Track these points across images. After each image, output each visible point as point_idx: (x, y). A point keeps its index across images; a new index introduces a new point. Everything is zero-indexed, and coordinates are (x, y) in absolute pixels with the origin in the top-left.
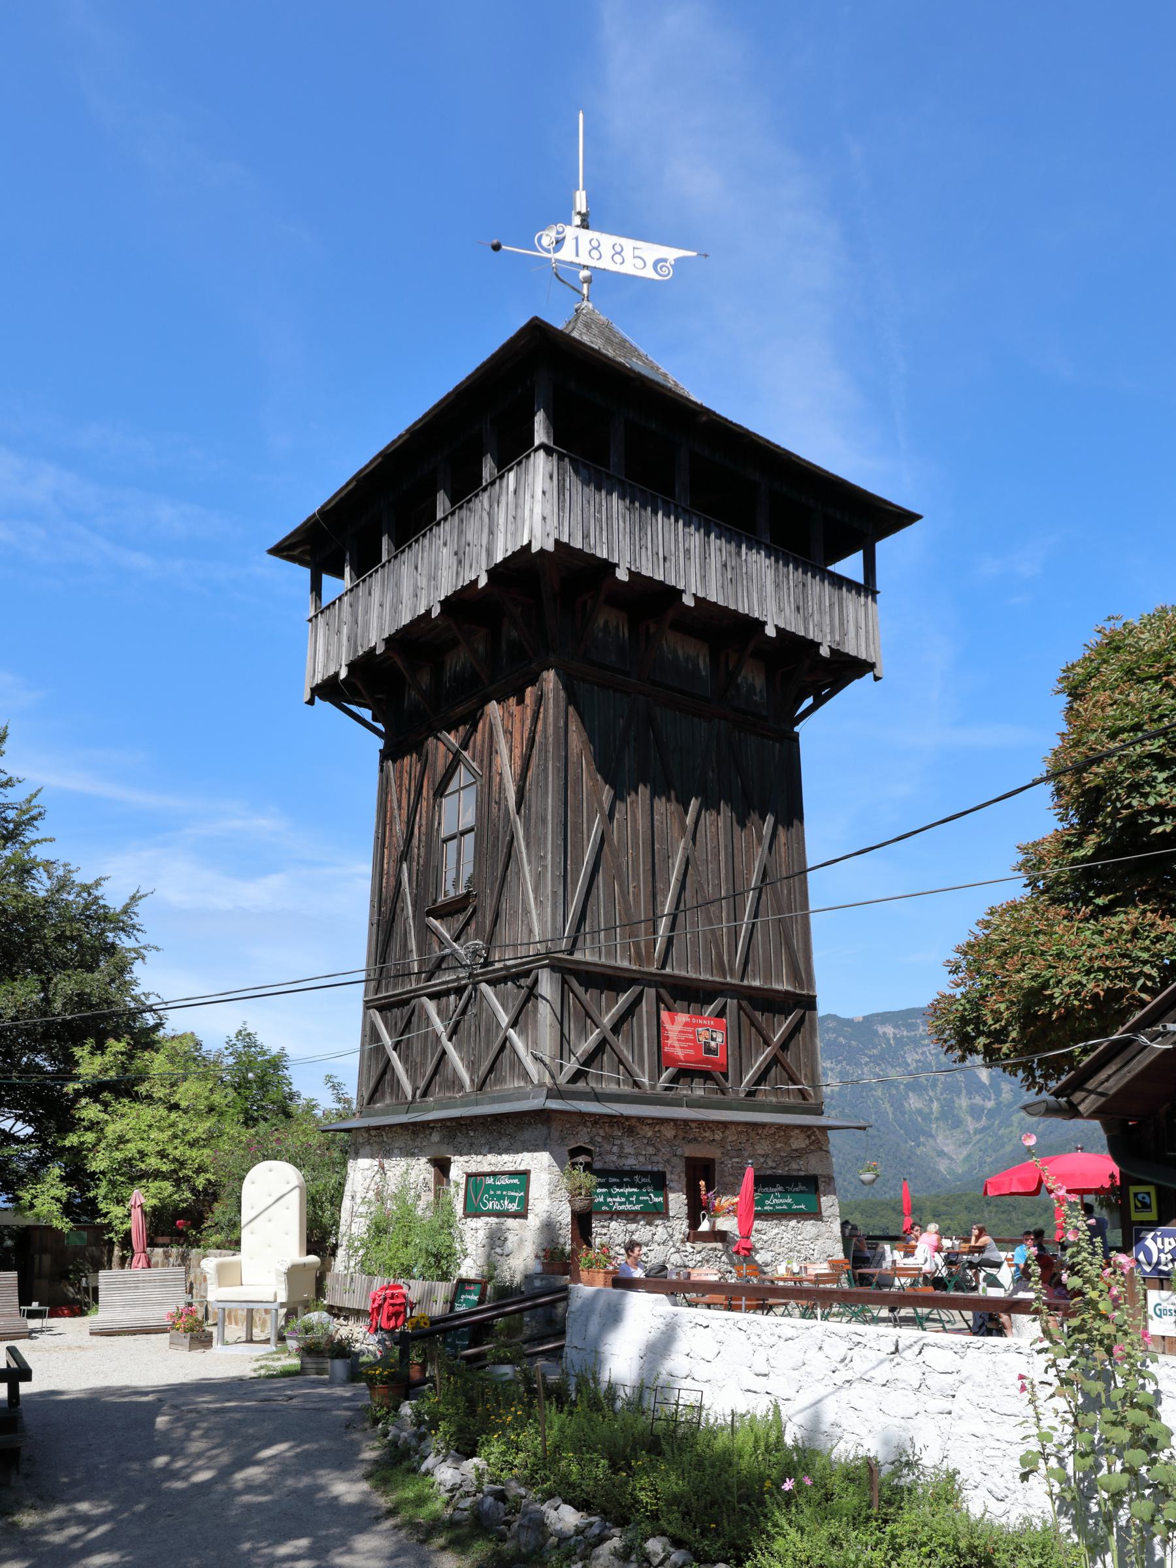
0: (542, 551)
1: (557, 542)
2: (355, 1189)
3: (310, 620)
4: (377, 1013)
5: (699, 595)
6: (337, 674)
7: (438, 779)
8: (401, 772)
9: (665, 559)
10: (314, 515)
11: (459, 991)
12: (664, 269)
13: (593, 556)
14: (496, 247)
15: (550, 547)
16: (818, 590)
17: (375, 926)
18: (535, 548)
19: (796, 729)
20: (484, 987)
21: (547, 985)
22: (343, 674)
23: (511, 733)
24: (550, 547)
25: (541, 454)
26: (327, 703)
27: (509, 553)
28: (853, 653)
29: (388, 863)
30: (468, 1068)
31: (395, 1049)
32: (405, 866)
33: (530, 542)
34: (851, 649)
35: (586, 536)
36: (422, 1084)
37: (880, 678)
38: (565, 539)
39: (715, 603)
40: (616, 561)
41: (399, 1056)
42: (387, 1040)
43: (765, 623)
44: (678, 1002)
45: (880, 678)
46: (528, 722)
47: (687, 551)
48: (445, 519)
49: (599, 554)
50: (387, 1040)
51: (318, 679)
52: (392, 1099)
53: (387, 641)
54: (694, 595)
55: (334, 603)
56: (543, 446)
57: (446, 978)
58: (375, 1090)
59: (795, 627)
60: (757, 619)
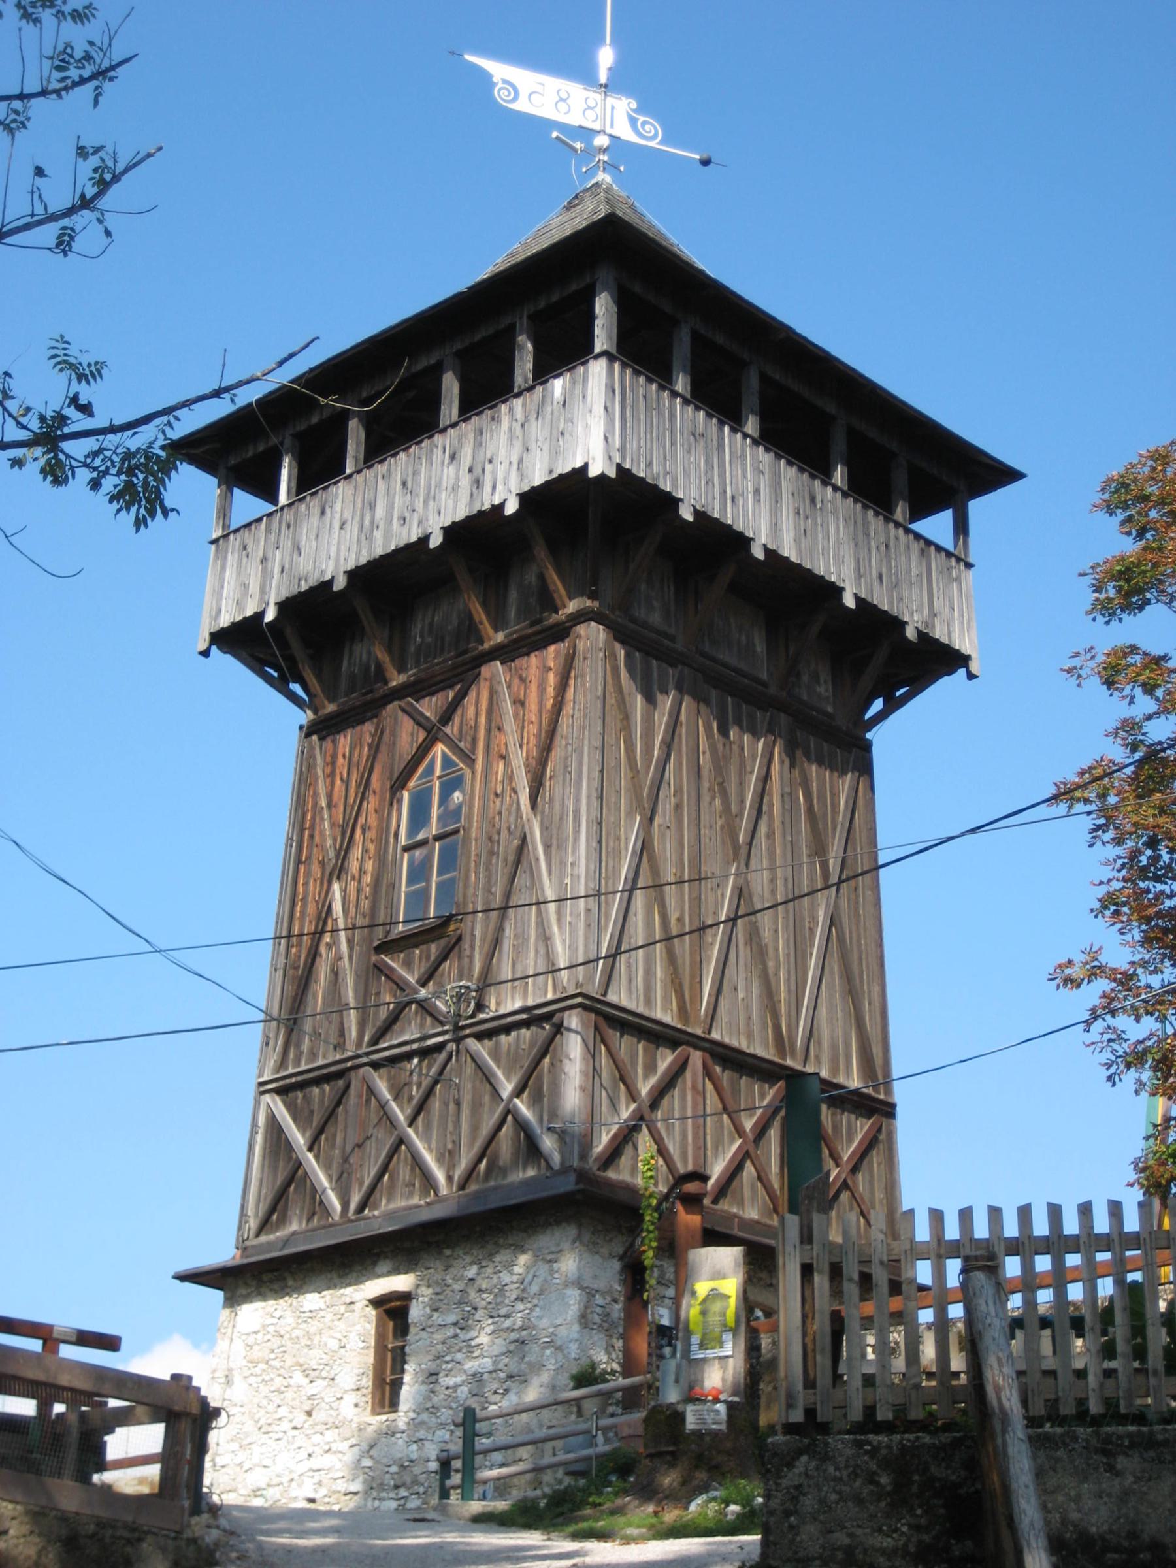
0: (602, 477)
1: (619, 466)
2: (232, 1365)
3: (215, 542)
4: (277, 1098)
5: (769, 546)
6: (260, 615)
7: (399, 767)
8: (334, 756)
9: (733, 498)
10: (250, 405)
11: (426, 1053)
12: (647, 127)
13: (656, 487)
14: (706, 162)
15: (612, 473)
16: (910, 560)
17: (280, 973)
18: (593, 472)
19: (869, 735)
20: (472, 1044)
21: (573, 1020)
22: (270, 616)
23: (522, 704)
24: (612, 473)
25: (602, 363)
26: (228, 656)
27: (555, 475)
28: (944, 639)
29: (306, 884)
30: (440, 1160)
31: (310, 1149)
32: (336, 887)
33: (586, 465)
34: (939, 633)
35: (649, 464)
36: (355, 1200)
37: (975, 677)
38: (627, 466)
39: (787, 558)
40: (680, 495)
41: (317, 1157)
42: (299, 1139)
43: (843, 589)
44: (727, 1072)
45: (975, 677)
46: (551, 691)
47: (757, 492)
48: (454, 425)
49: (662, 486)
50: (299, 1139)
51: (225, 621)
52: (300, 1223)
53: (352, 575)
54: (765, 545)
55: (259, 520)
56: (604, 353)
57: (409, 1033)
58: (272, 1210)
59: (882, 600)
60: (833, 583)
